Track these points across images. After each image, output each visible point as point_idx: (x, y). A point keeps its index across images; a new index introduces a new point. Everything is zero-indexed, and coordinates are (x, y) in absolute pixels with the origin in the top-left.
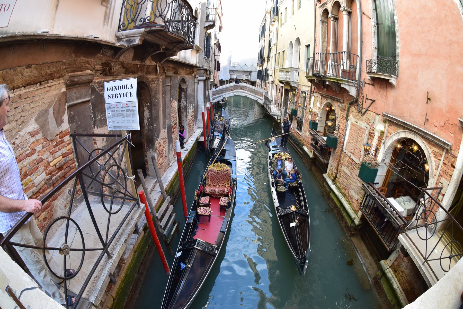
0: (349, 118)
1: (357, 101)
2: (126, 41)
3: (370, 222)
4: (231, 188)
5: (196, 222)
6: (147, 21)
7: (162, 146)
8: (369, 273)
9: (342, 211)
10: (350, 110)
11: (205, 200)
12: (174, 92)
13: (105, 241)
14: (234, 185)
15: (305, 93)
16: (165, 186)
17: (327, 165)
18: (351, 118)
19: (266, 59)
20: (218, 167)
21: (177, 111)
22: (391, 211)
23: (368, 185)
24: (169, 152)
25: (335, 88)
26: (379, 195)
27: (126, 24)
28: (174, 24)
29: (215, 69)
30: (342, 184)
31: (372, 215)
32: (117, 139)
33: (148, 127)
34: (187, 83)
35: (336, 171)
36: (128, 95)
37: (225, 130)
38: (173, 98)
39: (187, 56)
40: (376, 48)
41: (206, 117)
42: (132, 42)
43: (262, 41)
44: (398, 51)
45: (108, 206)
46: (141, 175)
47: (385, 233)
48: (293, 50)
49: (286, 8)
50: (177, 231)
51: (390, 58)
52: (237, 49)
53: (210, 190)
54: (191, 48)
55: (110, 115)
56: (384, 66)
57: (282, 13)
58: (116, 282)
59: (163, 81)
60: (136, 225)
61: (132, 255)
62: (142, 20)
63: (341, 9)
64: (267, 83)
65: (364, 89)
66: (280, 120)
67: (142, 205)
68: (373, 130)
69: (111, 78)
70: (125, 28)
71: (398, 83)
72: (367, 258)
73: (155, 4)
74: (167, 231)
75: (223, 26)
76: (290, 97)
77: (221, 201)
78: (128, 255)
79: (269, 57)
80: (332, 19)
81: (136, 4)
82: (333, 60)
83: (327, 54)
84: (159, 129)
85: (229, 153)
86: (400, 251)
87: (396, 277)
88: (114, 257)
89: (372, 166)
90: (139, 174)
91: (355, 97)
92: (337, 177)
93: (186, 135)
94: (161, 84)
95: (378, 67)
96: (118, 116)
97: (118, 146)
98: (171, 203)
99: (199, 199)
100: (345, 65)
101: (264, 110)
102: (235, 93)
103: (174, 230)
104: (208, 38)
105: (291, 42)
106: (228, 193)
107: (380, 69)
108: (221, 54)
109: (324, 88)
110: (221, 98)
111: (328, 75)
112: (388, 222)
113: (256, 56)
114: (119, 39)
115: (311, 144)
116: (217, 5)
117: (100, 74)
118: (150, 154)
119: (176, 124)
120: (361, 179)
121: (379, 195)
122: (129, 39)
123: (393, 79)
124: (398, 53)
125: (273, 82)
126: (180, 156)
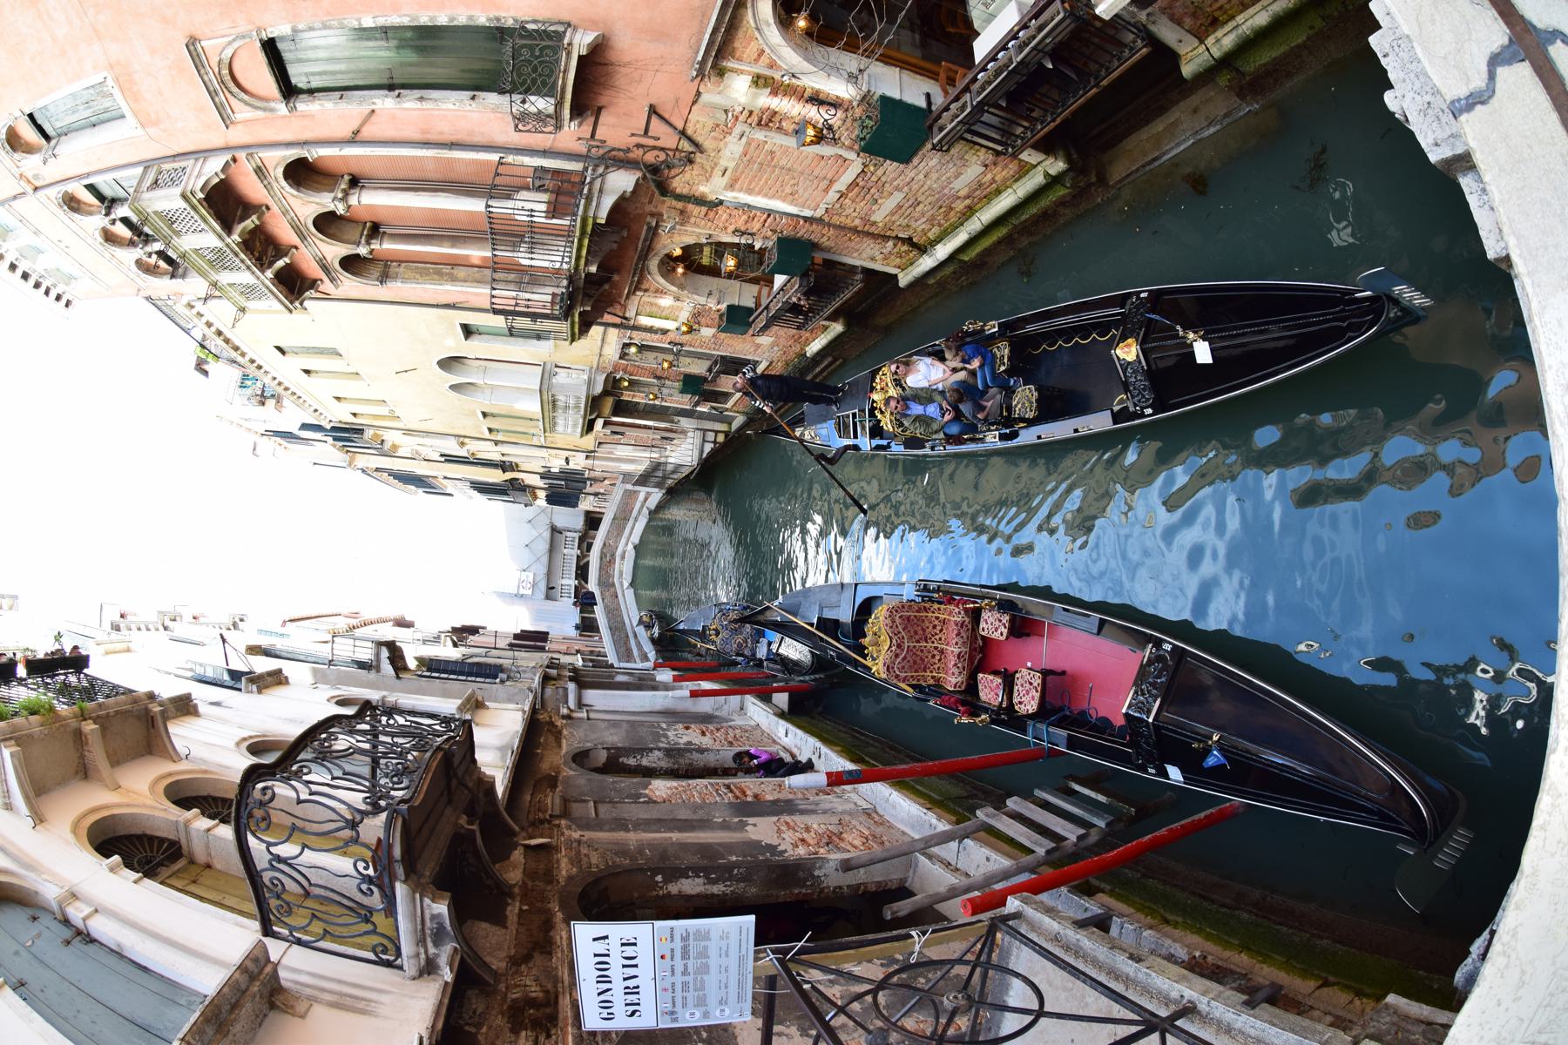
0: (712, 197)
1: (654, 169)
2: (436, 944)
3: (1058, 121)
4: (950, 601)
5: (1065, 717)
6: (371, 872)
7: (805, 835)
8: (1226, 115)
9: (1023, 218)
10: (685, 191)
11: (990, 690)
12: (620, 791)
13: (1134, 1029)
14: (938, 590)
15: (626, 346)
16: (943, 826)
17: (869, 273)
18: (712, 188)
19: (509, 475)
20: (877, 644)
21: (684, 783)
22: (1021, 48)
23: (935, 129)
24: (825, 812)
25: (610, 244)
26: (966, 89)
27: (375, 940)
28: (382, 782)
29: (542, 649)
30: (931, 221)
31: (1034, 114)
32: (784, 989)
33: (738, 881)
34: (589, 745)
35: (890, 243)
36: (630, 951)
37: (753, 618)
38: (639, 796)
39: (496, 741)
40: (473, 98)
41: (706, 685)
42: (441, 927)
43: (449, 487)
44: (482, 20)
45: (1011, 1023)
46: (904, 907)
47: (1093, 66)
48: (480, 382)
49: (338, 399)
50: (1095, 780)
51: (508, 48)
52: (473, 573)
53: (956, 671)
54: (467, 726)
55: (698, 1014)
56: (535, 70)
57: (355, 415)
58: (1273, 984)
59: (581, 827)
60: (1081, 924)
61: (1177, 933)
62: (364, 887)
63: (340, 209)
64: (593, 474)
65: (611, 143)
66: (717, 432)
67: (1013, 904)
68: (751, 113)
69: (565, 1002)
70: (390, 946)
71: (592, 24)
72: (1175, 124)
73: (311, 840)
74: (1097, 815)
75: (396, 613)
76: (640, 398)
77: (996, 636)
78: (1178, 945)
79: (504, 466)
80: (375, 245)
81: (309, 903)
82: (515, 247)
83: (495, 266)
84: (744, 843)
85: (832, 607)
86: (1149, 10)
87: (1232, 17)
88: (1189, 994)
89: (869, 117)
90: (901, 914)
91: (639, 174)
92: (910, 239)
93: (763, 751)
94: (588, 835)
95: (538, 93)
96: (702, 988)
97: (806, 986)
98: (999, 805)
99: (986, 710)
100: (530, 206)
101: (681, 489)
102: (626, 584)
103: (1093, 794)
104: (433, 667)
105: (453, 387)
106: (966, 610)
107: (544, 84)
108: (491, 628)
109: (609, 280)
110: (641, 630)
111: (565, 266)
112: (1055, 55)
113: (497, 508)
114: (429, 968)
115: (799, 328)
116: (322, 629)
117: (549, 1036)
118: (831, 876)
119: (728, 787)
120: (914, 153)
121: (966, 89)
122: (429, 934)
123: (576, 42)
124: (489, 20)
125: (590, 454)
126: (839, 774)
